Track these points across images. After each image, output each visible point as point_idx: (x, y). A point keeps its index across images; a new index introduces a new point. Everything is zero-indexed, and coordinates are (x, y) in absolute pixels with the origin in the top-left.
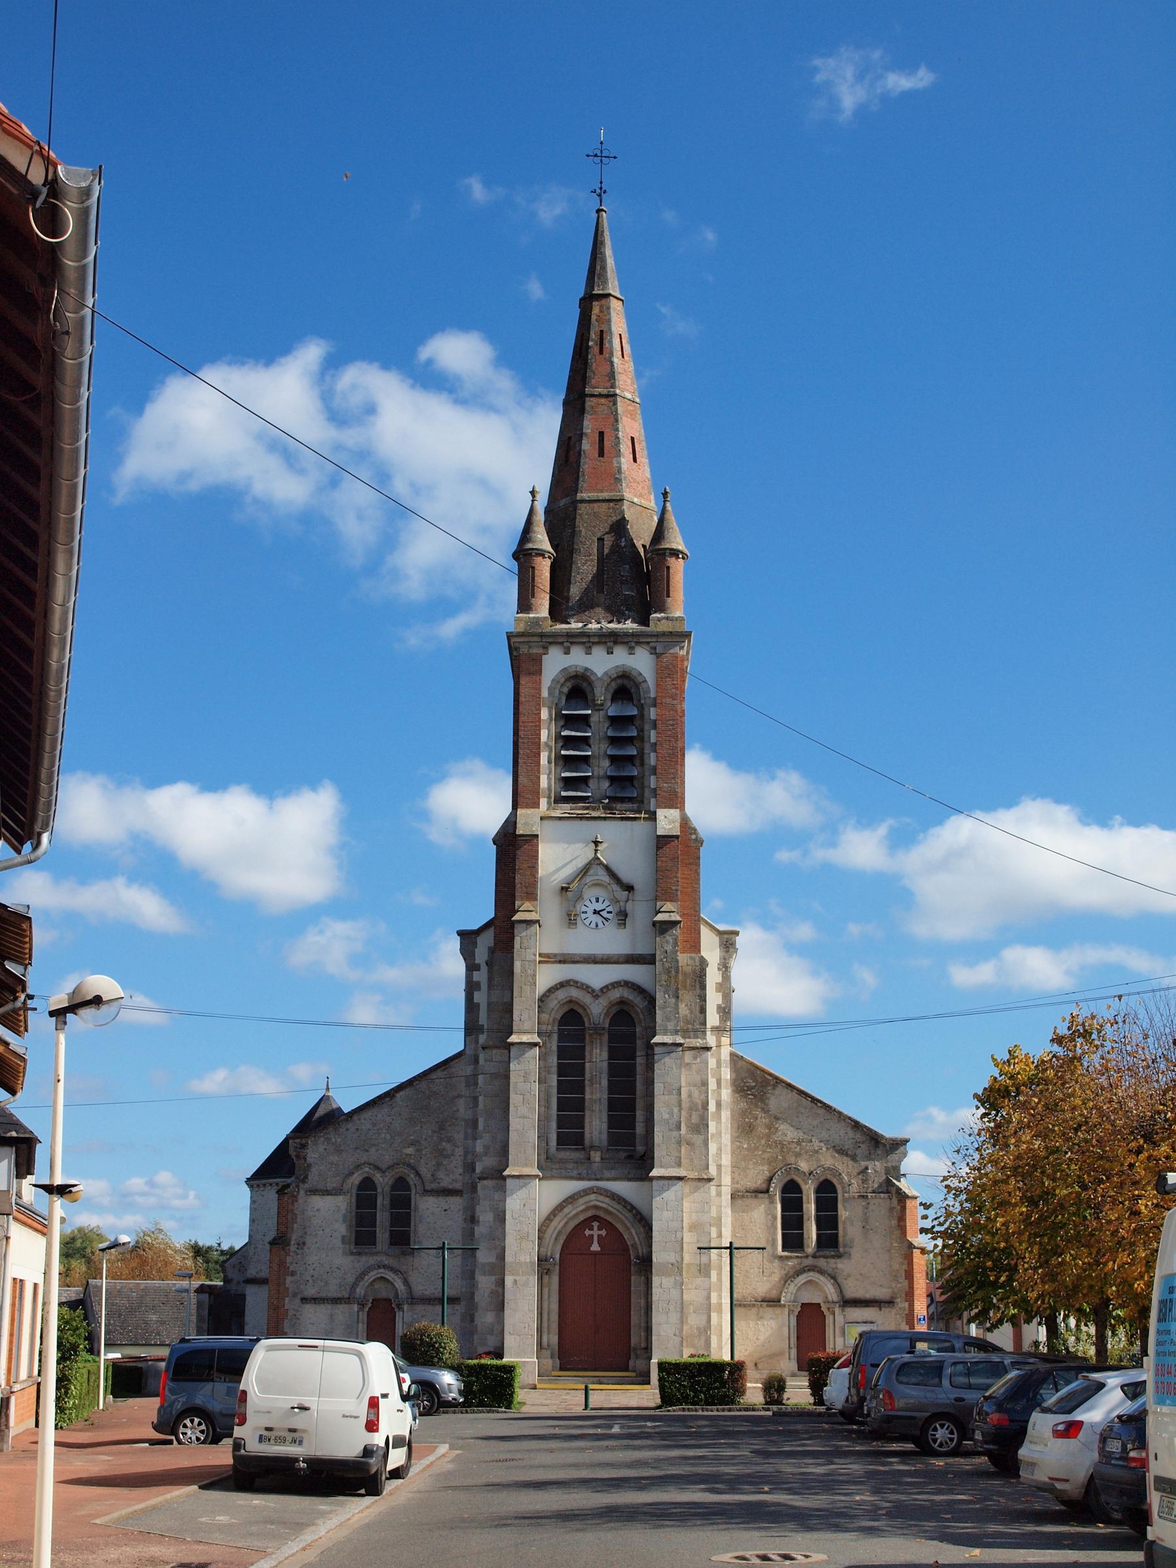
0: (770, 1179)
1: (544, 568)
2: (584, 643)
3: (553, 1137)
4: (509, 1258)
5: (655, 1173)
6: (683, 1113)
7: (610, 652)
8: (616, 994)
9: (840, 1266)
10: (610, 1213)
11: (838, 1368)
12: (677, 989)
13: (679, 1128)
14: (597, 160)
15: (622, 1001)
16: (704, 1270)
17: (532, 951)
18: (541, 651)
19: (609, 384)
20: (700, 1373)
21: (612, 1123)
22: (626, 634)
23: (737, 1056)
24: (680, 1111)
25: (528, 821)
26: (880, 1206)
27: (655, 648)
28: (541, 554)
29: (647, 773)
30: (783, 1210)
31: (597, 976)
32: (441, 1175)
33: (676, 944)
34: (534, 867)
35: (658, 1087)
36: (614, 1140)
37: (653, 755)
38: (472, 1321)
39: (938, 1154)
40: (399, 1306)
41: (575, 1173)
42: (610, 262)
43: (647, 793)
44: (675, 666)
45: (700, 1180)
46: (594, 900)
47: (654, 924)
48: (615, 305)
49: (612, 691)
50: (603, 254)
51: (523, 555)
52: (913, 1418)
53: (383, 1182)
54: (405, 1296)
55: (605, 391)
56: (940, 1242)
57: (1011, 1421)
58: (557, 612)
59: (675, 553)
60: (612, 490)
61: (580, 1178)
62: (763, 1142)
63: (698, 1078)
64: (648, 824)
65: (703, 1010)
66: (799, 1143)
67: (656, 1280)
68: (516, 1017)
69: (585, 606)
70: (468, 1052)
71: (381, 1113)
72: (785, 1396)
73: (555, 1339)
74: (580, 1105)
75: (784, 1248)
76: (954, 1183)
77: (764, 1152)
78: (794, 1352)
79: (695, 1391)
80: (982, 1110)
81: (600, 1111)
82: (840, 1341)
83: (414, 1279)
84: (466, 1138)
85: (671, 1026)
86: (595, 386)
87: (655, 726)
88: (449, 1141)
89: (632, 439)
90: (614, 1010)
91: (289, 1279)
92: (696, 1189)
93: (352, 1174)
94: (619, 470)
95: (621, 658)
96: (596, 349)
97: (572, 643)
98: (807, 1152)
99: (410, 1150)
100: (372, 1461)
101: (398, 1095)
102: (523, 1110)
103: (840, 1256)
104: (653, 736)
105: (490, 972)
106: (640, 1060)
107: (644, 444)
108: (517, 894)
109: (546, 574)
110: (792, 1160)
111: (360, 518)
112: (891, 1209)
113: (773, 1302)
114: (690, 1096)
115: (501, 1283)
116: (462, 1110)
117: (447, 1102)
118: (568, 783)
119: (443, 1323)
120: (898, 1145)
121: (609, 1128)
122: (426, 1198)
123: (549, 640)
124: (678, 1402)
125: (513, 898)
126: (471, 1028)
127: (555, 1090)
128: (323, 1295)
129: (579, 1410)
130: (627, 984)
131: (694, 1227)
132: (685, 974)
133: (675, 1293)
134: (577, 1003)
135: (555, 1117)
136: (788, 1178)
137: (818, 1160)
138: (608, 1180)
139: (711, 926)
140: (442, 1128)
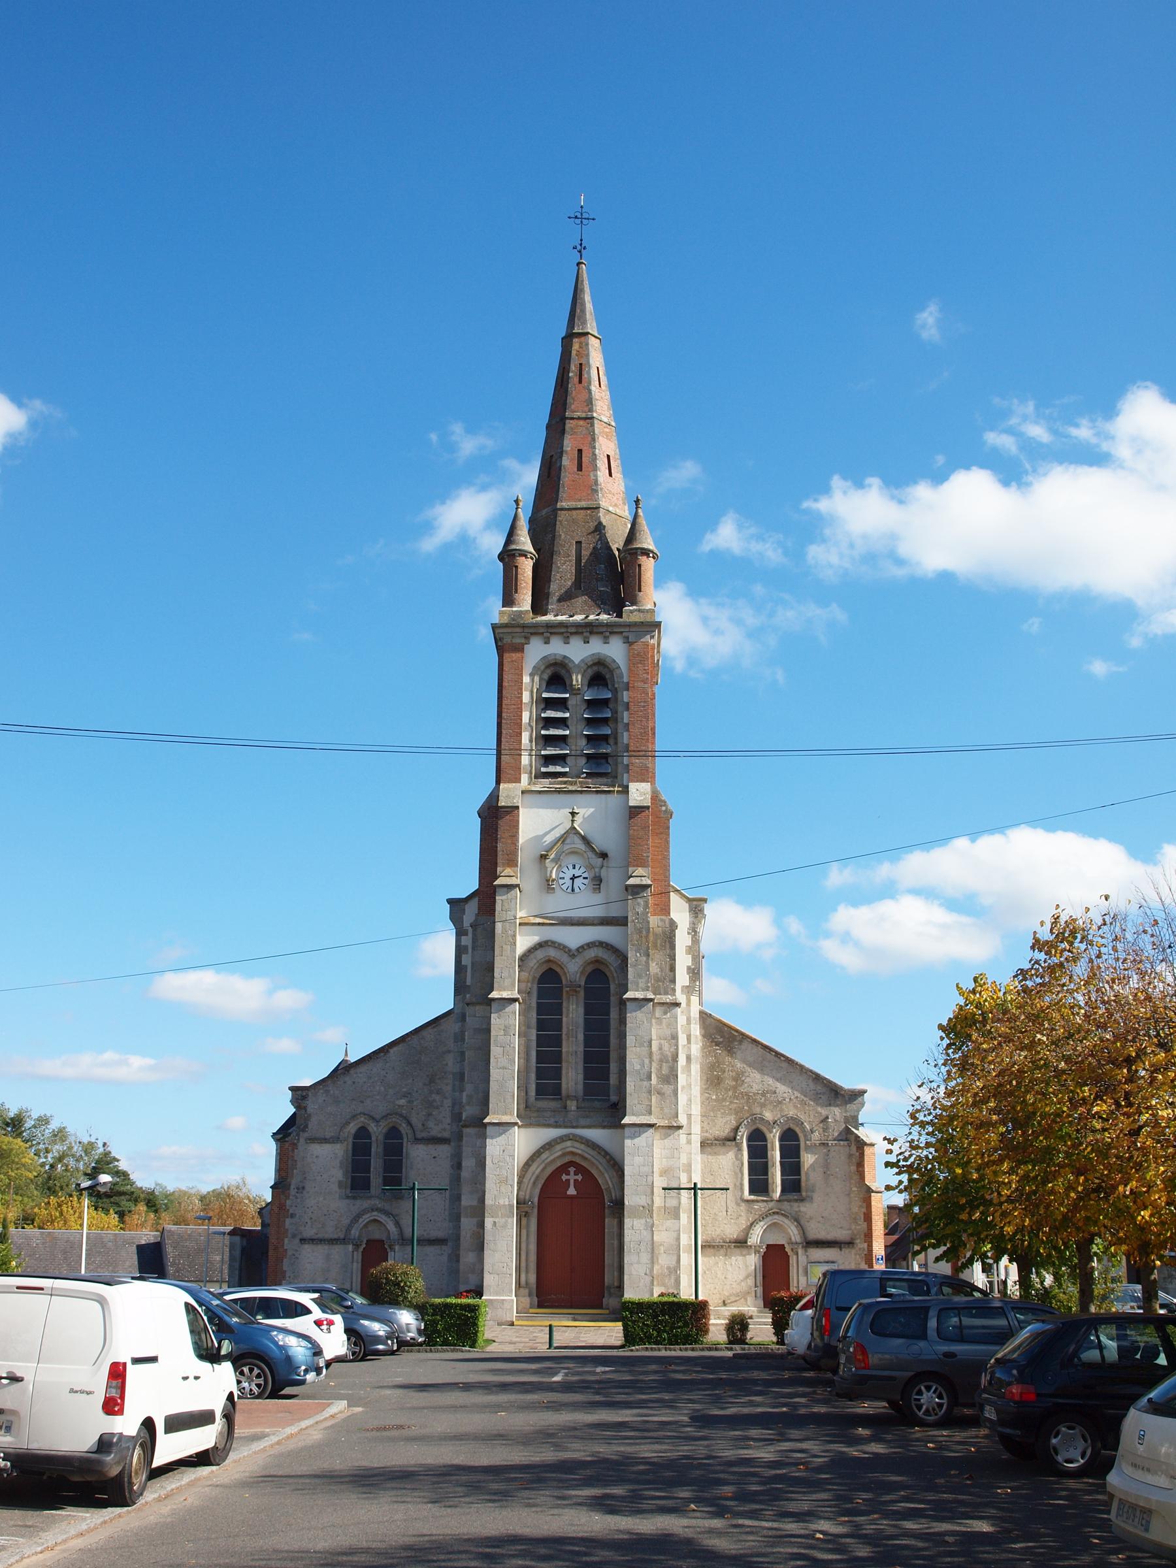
0: (736, 1129)
1: (526, 568)
2: (562, 633)
3: (533, 1087)
5: (626, 1120)
6: (654, 1065)
8: (592, 954)
9: (802, 1209)
10: (586, 1159)
14: (578, 221)
15: (597, 961)
16: (675, 1213)
17: (512, 913)
18: (523, 641)
19: (586, 409)
20: (663, 1313)
21: (588, 1074)
23: (706, 1014)
25: (510, 793)
26: (840, 1154)
27: (627, 638)
28: (524, 554)
31: (573, 937)
32: (431, 1124)
33: (646, 906)
34: (515, 836)
35: (630, 1040)
36: (589, 1091)
38: (458, 1261)
39: (897, 1094)
41: (552, 1121)
42: (589, 306)
44: (646, 653)
45: (670, 1127)
46: (571, 867)
47: (627, 888)
48: (594, 343)
51: (508, 556)
53: (377, 1131)
55: (584, 415)
57: (1038, 1395)
58: (539, 606)
59: (646, 552)
62: (730, 1093)
63: (668, 1032)
65: (673, 969)
66: (763, 1094)
67: (628, 1222)
69: (566, 597)
71: (376, 1067)
73: (533, 1278)
74: (558, 1058)
75: (751, 1192)
76: (921, 1116)
78: (760, 1290)
79: (659, 1332)
80: (946, 1041)
82: (803, 1280)
83: (406, 1221)
84: (454, 1090)
86: (575, 409)
90: (589, 969)
91: (288, 1221)
92: (666, 1136)
93: (348, 1123)
95: (596, 647)
96: (576, 380)
99: (402, 1102)
100: (109, 1458)
101: (392, 1051)
102: (503, 1062)
103: (802, 1200)
105: (474, 935)
106: (614, 1015)
108: (499, 861)
110: (758, 1110)
112: (850, 1156)
113: (741, 1243)
114: (660, 1049)
115: (481, 1225)
116: (450, 1064)
118: (548, 760)
120: (856, 1095)
124: (642, 1341)
125: (496, 865)
126: (460, 988)
127: (534, 1044)
128: (320, 1236)
129: (542, 1349)
131: (664, 1172)
132: (655, 935)
133: (646, 1234)
134: (555, 962)
135: (534, 1069)
136: (754, 1127)
137: (782, 1110)
138: (583, 1127)
140: (432, 1081)
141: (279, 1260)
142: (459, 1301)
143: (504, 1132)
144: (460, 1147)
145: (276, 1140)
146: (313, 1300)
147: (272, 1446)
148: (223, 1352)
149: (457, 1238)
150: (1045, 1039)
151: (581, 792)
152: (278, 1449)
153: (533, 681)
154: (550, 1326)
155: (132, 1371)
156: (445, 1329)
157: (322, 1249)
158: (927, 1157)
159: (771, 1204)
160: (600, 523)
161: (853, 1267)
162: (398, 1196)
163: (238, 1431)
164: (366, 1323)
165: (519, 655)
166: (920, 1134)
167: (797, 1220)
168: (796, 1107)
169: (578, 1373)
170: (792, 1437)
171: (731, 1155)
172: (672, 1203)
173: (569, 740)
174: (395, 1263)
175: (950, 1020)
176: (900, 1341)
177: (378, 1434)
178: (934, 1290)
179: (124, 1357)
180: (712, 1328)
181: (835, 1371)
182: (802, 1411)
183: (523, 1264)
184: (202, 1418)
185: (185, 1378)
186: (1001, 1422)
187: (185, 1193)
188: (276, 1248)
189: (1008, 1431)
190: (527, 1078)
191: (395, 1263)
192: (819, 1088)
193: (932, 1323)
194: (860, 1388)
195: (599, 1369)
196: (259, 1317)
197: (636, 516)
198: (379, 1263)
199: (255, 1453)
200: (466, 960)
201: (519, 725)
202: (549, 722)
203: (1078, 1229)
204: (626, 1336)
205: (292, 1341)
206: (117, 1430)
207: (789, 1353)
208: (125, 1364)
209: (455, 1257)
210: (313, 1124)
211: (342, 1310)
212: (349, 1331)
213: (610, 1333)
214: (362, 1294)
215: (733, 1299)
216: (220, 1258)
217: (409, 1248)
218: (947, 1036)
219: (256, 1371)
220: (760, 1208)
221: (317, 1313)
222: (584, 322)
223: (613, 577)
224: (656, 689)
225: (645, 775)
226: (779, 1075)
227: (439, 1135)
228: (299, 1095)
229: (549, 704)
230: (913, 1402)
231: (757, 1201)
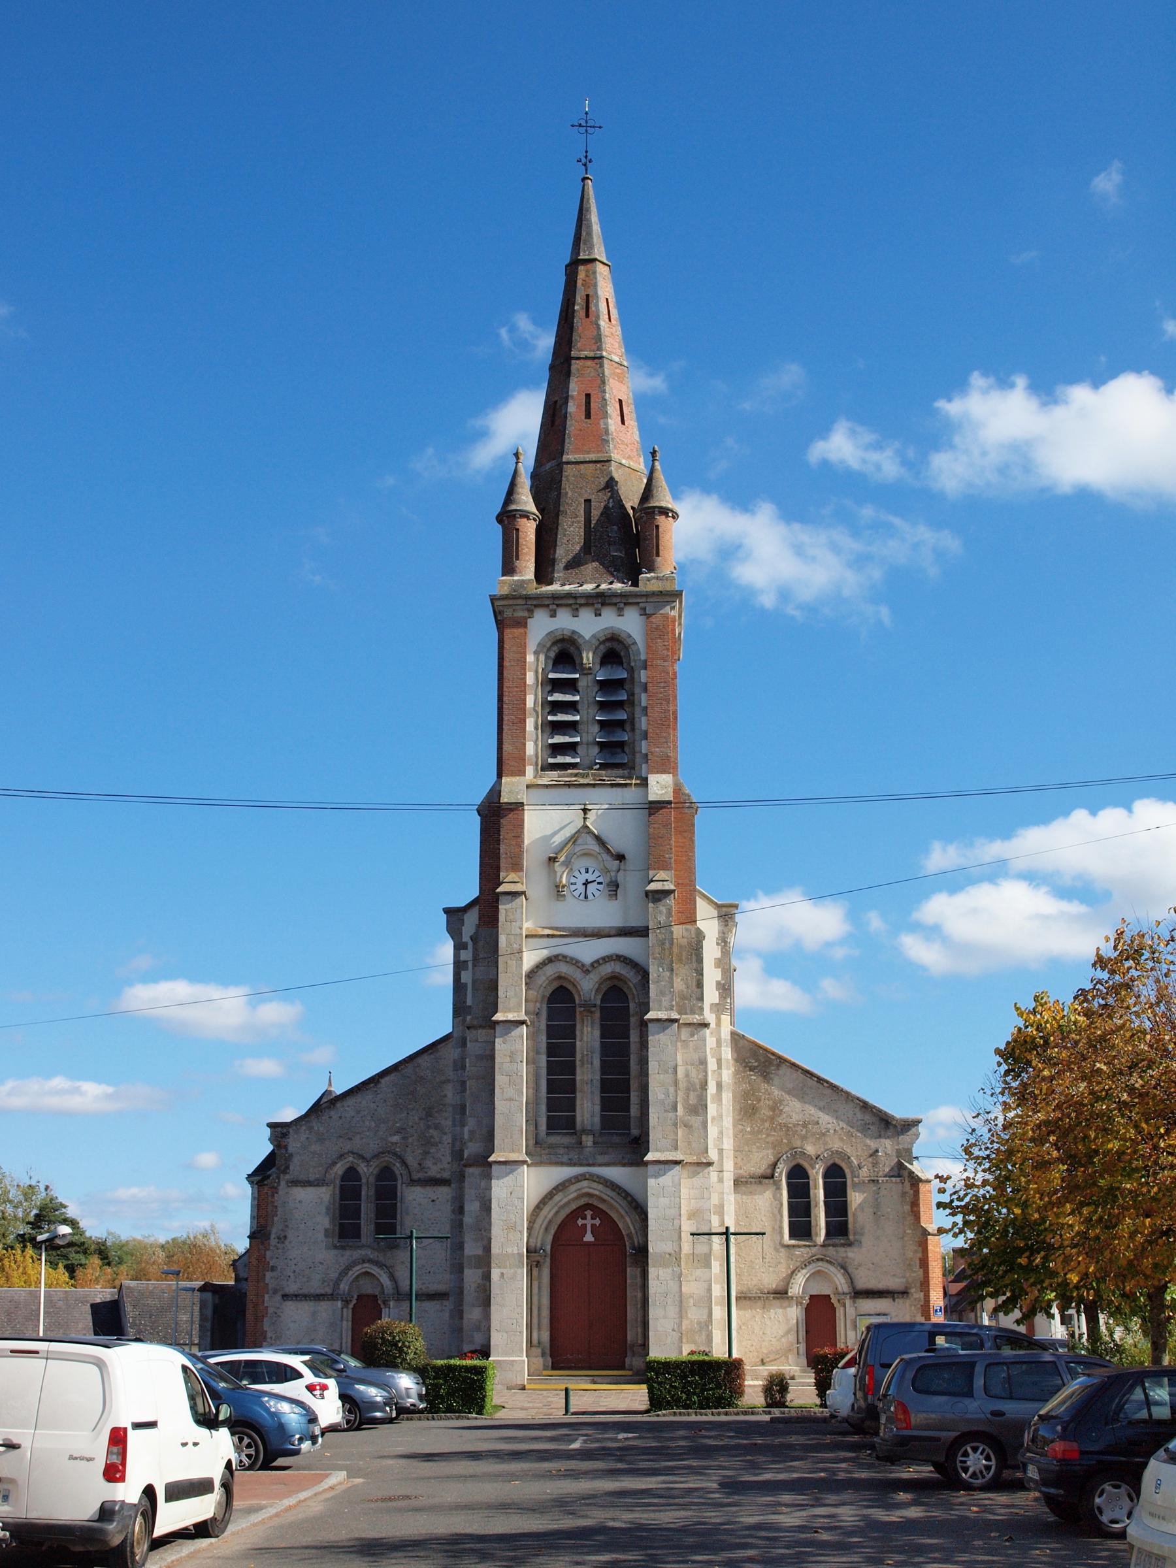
0: (775, 1165)
1: (528, 531)
3: (543, 1122)
4: (495, 1249)
5: (649, 1157)
6: (681, 1094)
7: (598, 614)
8: (608, 969)
9: (850, 1255)
10: (604, 1201)
11: (844, 1367)
12: (672, 962)
13: (675, 1109)
14: (583, 130)
15: (614, 977)
16: (706, 1261)
17: (518, 924)
18: (526, 614)
19: (595, 347)
21: (606, 1105)
22: (615, 595)
23: (738, 1035)
24: (676, 1091)
25: (513, 789)
26: (892, 1191)
27: (645, 609)
28: (526, 515)
29: (637, 737)
30: (790, 1197)
31: (588, 951)
32: (428, 1163)
34: (519, 836)
35: (653, 1066)
36: (607, 1123)
37: (644, 719)
38: (461, 1318)
39: (952, 1127)
40: (385, 1302)
41: (565, 1159)
42: (596, 228)
43: (638, 759)
45: (699, 1164)
46: (583, 871)
47: (647, 893)
48: (602, 271)
49: (600, 654)
50: (589, 220)
51: (508, 518)
52: (937, 1439)
54: (391, 1291)
55: (591, 354)
56: (959, 1219)
57: (1082, 1453)
58: (543, 574)
60: (598, 452)
61: (571, 1163)
62: (767, 1125)
63: (696, 1057)
64: (640, 790)
65: (700, 985)
66: (805, 1125)
67: (652, 1272)
68: (500, 994)
69: (574, 564)
70: (455, 1035)
71: (364, 1101)
72: (789, 1397)
73: (546, 1336)
74: (571, 1087)
75: (792, 1235)
76: (976, 1152)
77: (768, 1135)
78: (803, 1347)
79: (689, 1394)
80: (1004, 1067)
81: (592, 1093)
83: (402, 1273)
84: (454, 1125)
85: (665, 1001)
87: (646, 690)
88: (436, 1128)
89: (620, 401)
91: (268, 1275)
94: (607, 432)
95: (609, 620)
96: (583, 313)
97: (558, 605)
98: (814, 1134)
99: (395, 1139)
100: (111, 1527)
101: (383, 1081)
102: (510, 1092)
103: (850, 1245)
104: (644, 699)
105: (475, 949)
106: (634, 1037)
107: (632, 407)
108: (502, 865)
109: (532, 536)
110: (798, 1143)
111: (818, 1202)
112: (904, 1194)
113: (781, 1294)
114: (687, 1075)
115: (487, 1277)
116: (450, 1095)
117: (435, 1091)
118: (556, 749)
119: (411, 1321)
121: (602, 1110)
122: (414, 1188)
123: (534, 603)
124: (669, 1405)
126: (459, 1009)
127: (544, 1072)
128: (305, 1291)
129: (558, 1415)
130: (621, 959)
131: (692, 1215)
132: (680, 946)
133: (673, 1286)
135: (545, 1100)
136: (794, 1163)
137: (825, 1143)
138: (600, 1165)
139: (705, 896)
140: (429, 1113)
141: (259, 1319)
142: (464, 1362)
143: (512, 1171)
144: (461, 1189)
145: (251, 1183)
146: (304, 1362)
147: (271, 1518)
148: (221, 1418)
149: (460, 1292)
150: (1104, 1068)
151: (594, 785)
152: (276, 1522)
153: (538, 660)
154: (567, 1390)
155: (133, 1436)
156: (448, 1394)
157: (307, 1307)
158: (984, 1196)
159: (814, 1250)
160: (612, 478)
161: (907, 1319)
162: (393, 1246)
163: (237, 1504)
164: (362, 1388)
165: (521, 630)
166: (976, 1172)
167: (843, 1267)
168: (841, 1139)
169: (598, 1440)
170: (828, 1502)
171: (768, 1194)
172: (701, 1248)
173: (580, 727)
174: (391, 1319)
175: (1008, 1043)
176: (943, 1398)
177: (384, 1504)
178: (988, 1344)
179: (125, 1423)
180: (747, 1390)
181: (877, 1434)
182: (842, 1476)
183: (535, 1321)
184: (200, 1487)
185: (184, 1445)
186: (1045, 1482)
187: (140, 1242)
188: (256, 1305)
189: (1052, 1491)
190: (537, 1116)
191: (391, 1319)
192: (868, 1118)
193: (979, 1382)
194: (904, 1449)
195: (621, 1436)
196: (245, 1382)
197: (652, 471)
198: (373, 1321)
199: (254, 1525)
200: (466, 977)
201: (523, 710)
202: (556, 707)
203: (1146, 1277)
204: (651, 1399)
205: (285, 1407)
206: (119, 1498)
207: (833, 1416)
208: (125, 1429)
209: (458, 1313)
210: (295, 1167)
211: (335, 1374)
212: (343, 1397)
213: (635, 1397)
214: (353, 1355)
215: (772, 1357)
216: (189, 1317)
217: (406, 1304)
218: (1005, 1061)
219: (246, 1440)
220: (803, 1252)
221: (309, 1377)
222: (591, 247)
223: (627, 538)
224: (677, 667)
225: (666, 765)
226: (822, 1104)
227: (438, 1176)
228: (279, 1131)
229: (557, 685)
230: (959, 1465)
231: (799, 1246)
